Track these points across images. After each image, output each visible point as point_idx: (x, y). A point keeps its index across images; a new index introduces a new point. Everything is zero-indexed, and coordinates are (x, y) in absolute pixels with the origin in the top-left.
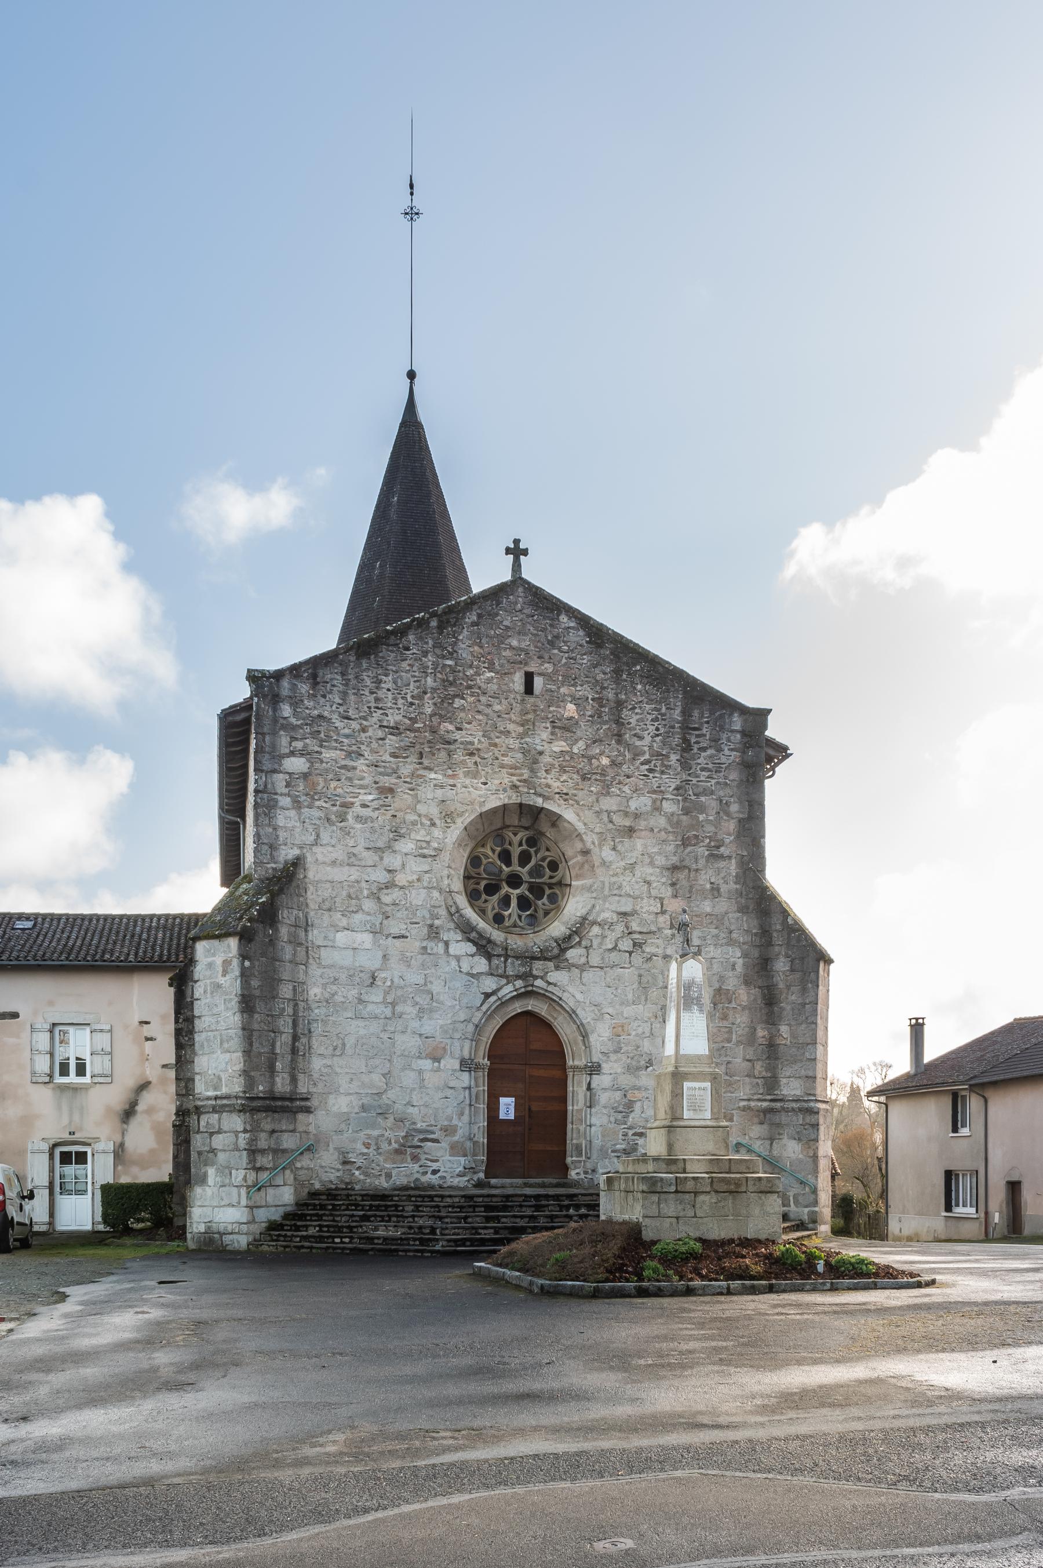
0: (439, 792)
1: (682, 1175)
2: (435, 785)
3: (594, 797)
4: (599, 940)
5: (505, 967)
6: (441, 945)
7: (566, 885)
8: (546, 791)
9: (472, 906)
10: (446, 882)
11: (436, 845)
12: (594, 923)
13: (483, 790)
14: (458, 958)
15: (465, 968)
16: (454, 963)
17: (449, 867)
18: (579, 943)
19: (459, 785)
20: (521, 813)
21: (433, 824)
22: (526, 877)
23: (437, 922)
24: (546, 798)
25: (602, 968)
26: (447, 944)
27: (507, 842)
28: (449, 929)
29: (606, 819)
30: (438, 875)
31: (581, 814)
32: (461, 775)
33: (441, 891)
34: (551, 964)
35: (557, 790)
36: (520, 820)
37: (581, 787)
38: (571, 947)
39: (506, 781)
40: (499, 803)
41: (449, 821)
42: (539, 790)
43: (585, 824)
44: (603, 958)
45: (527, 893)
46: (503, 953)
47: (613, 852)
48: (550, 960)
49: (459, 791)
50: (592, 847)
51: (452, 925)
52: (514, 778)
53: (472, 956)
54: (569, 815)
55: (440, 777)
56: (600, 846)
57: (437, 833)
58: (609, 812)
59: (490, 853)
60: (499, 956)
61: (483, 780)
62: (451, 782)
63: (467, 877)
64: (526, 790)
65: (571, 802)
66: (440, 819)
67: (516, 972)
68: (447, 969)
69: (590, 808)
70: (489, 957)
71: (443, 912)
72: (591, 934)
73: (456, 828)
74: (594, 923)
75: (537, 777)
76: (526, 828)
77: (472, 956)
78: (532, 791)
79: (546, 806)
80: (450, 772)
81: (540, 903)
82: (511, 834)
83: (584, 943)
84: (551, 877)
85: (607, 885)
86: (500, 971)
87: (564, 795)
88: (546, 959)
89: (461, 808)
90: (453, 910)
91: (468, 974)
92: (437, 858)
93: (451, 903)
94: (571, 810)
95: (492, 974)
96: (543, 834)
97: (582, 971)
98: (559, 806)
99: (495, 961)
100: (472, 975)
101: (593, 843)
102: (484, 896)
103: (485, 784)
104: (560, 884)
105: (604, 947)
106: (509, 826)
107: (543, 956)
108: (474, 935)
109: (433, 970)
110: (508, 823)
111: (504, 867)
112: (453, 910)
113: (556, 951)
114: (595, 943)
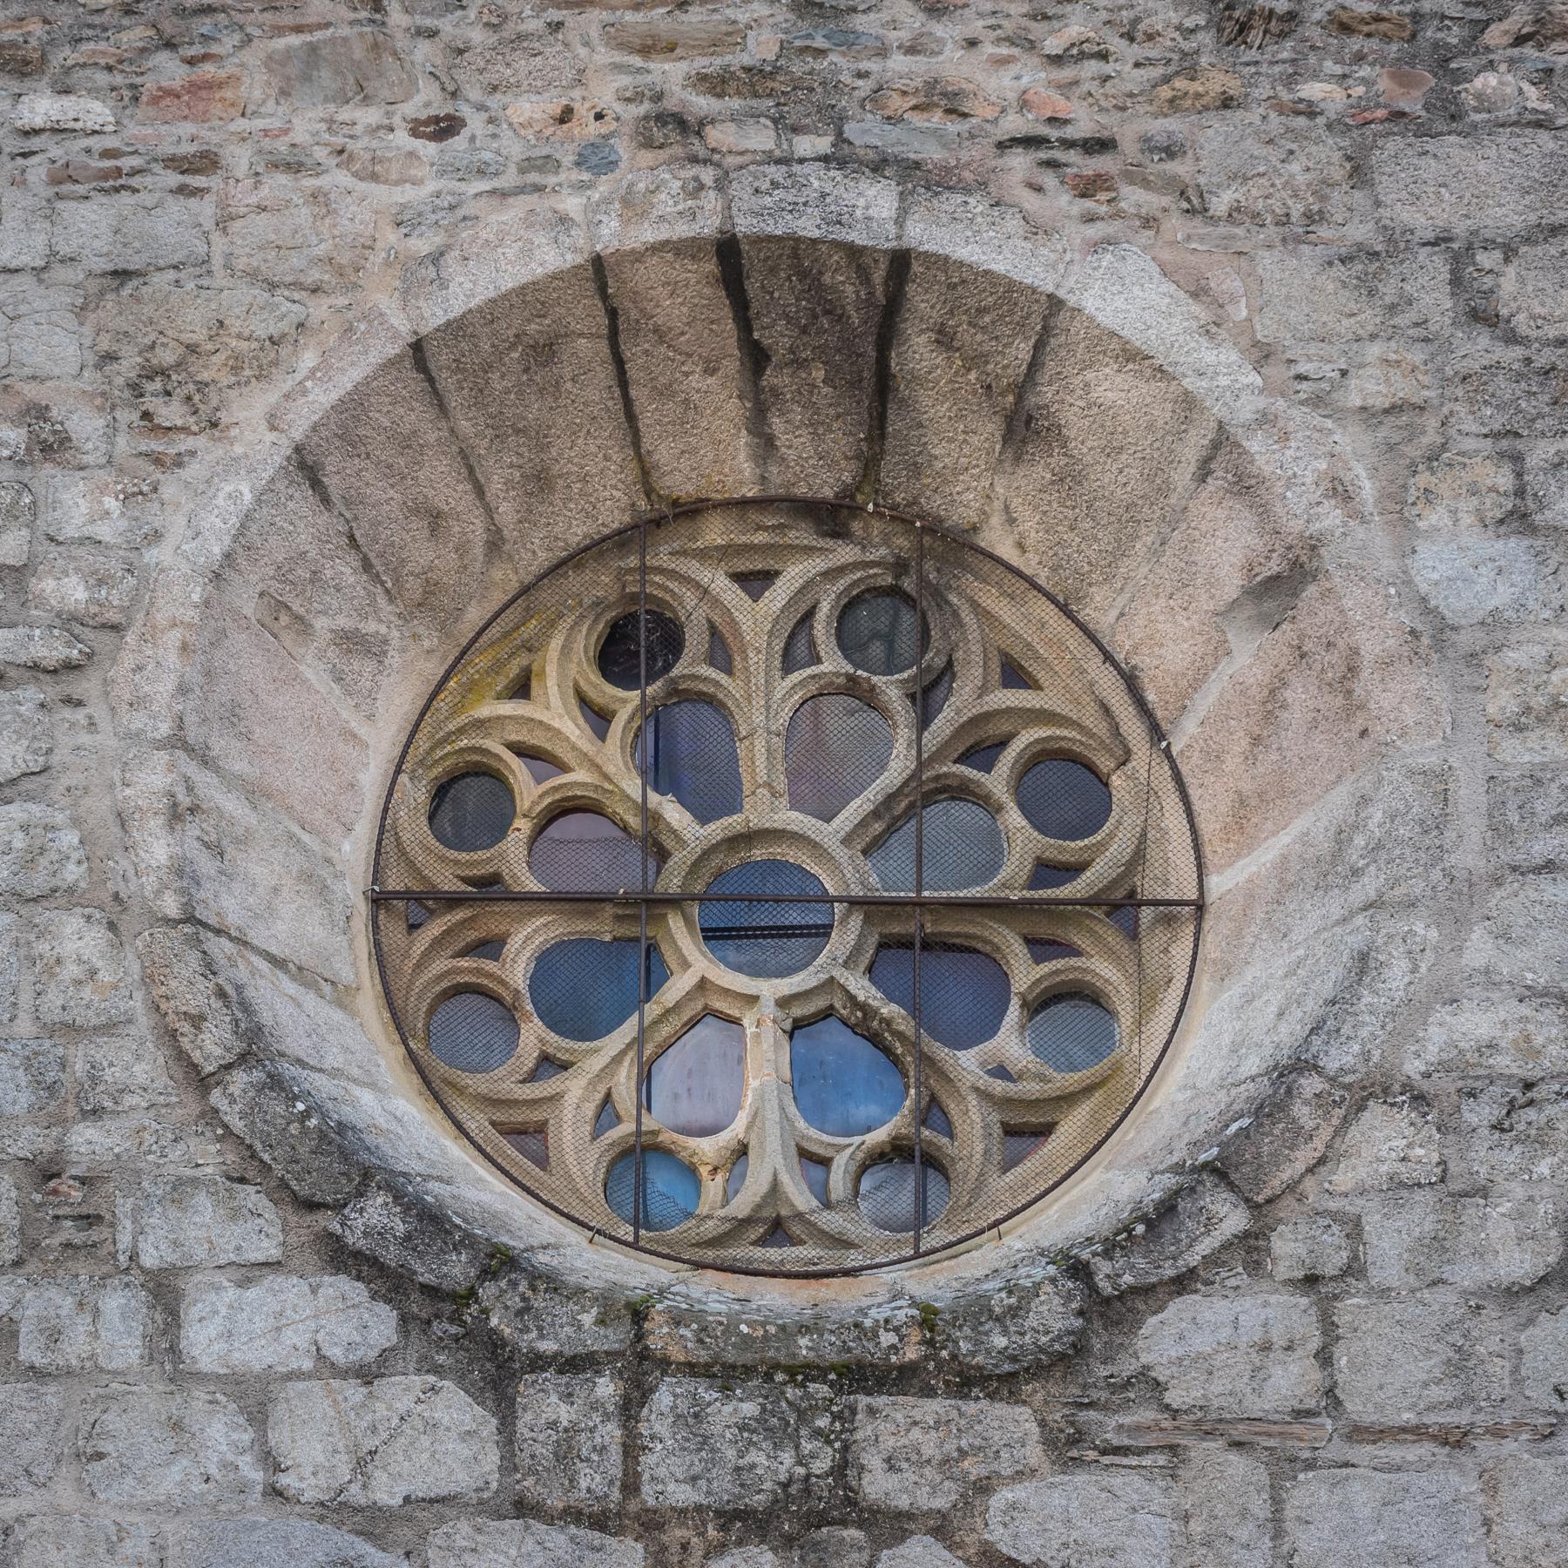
0: (92, 226)
1: (643, 673)
2: (63, 176)
3: (1328, 153)
4: (1421, 1215)
5: (632, 1449)
6: (120, 1306)
7: (1169, 913)
8: (926, 138)
9: (435, 1091)
10: (158, 849)
11: (76, 593)
12: (1363, 1094)
13: (425, 174)
14: (255, 1398)
15: (313, 1453)
16: (221, 1434)
17: (178, 742)
18: (1250, 1248)
19: (239, 158)
20: (756, 357)
21: (52, 446)
22: (843, 872)
23: (88, 1142)
24: (917, 179)
25: (1455, 1440)
26: (165, 1293)
27: (695, 640)
28: (181, 1190)
29: (1433, 297)
30: (98, 806)
31: (1226, 281)
32: (255, 86)
33: (115, 916)
34: (1013, 1425)
35: (1015, 124)
36: (766, 446)
37: (1216, 82)
38: (1183, 1283)
39: (605, 92)
40: (552, 257)
41: (171, 413)
42: (866, 132)
43: (1262, 354)
44: (1461, 1364)
45: (861, 987)
46: (615, 1338)
47: (1514, 547)
48: (1002, 1383)
49: (243, 196)
50: (1331, 517)
51: (209, 1156)
52: (671, 74)
53: (367, 1374)
54: (1121, 292)
55: (97, 112)
56: (1401, 509)
57: (79, 504)
58: (1458, 253)
59: (571, 728)
60: (577, 1364)
61: (426, 100)
62: (180, 136)
63: (395, 903)
64: (762, 138)
65: (1133, 197)
66: (107, 404)
67: (723, 1488)
68: (170, 1481)
69: (1301, 228)
70: (498, 1373)
71: (137, 1066)
72: (1344, 1177)
73: (231, 466)
74: (1363, 1094)
75: (848, 41)
76: (831, 517)
77: (367, 1374)
78: (806, 145)
79: (923, 234)
80: (169, 69)
81: (968, 1063)
82: (719, 582)
83: (1289, 1248)
84: (1048, 871)
85: (1469, 795)
86: (594, 1481)
87: (1075, 157)
88: (968, 1381)
89: (252, 315)
90: (212, 1045)
91: (334, 1510)
92: (86, 685)
93: (197, 997)
94: (1136, 261)
95: (523, 1508)
96: (957, 546)
97: (1286, 1467)
98: (1036, 229)
99: (547, 1406)
100: (373, 1523)
101: (1340, 491)
102: (534, 1035)
103: (443, 128)
104: (1122, 905)
105: (1467, 1274)
106: (691, 511)
107: (944, 1362)
108: (375, 1214)
109: (65, 1494)
110: (680, 482)
111: (673, 813)
112: (212, 1045)
113: (1052, 1316)
114: (1390, 1243)
